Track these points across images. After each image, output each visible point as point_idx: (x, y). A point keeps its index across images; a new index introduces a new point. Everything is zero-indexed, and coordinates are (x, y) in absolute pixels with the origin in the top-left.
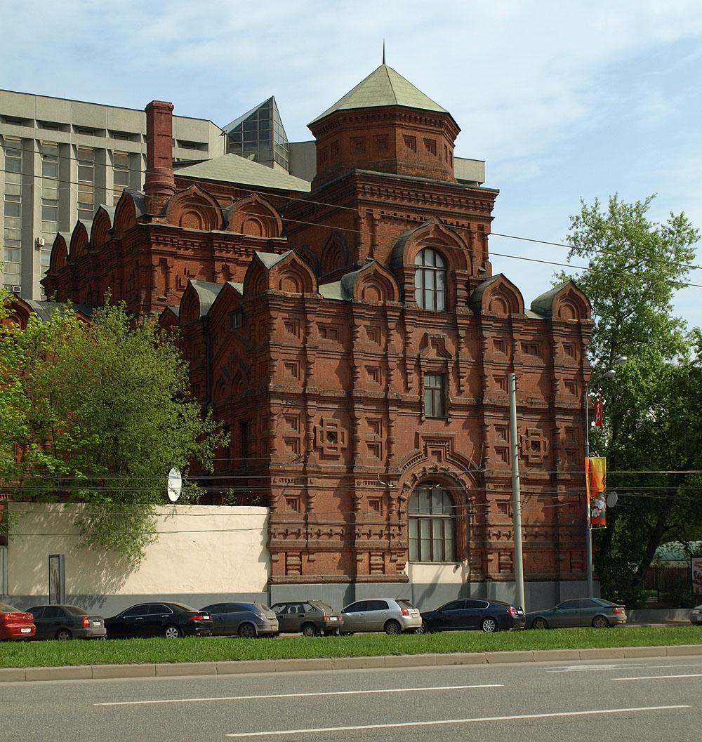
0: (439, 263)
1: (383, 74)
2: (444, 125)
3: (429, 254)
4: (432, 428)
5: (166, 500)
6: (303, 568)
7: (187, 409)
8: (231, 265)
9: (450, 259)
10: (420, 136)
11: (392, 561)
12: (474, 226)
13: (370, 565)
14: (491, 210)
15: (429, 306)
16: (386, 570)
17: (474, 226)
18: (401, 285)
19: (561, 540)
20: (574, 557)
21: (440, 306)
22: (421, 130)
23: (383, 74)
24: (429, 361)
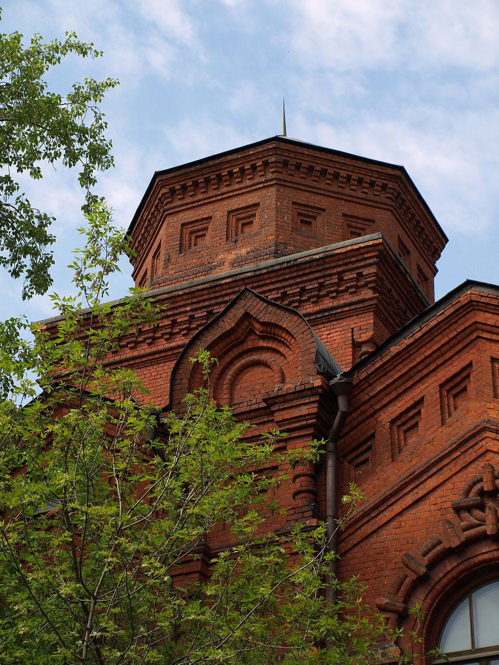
22: (339, 197)
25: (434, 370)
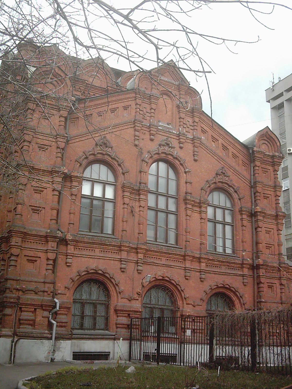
25: (128, 98)
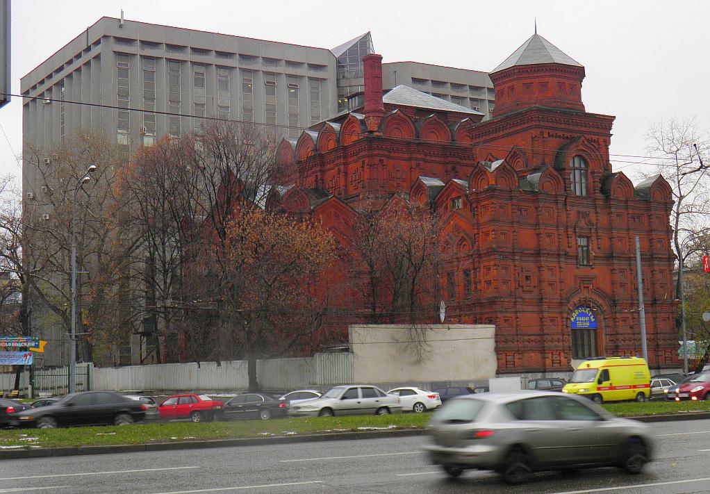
0: (583, 166)
1: (536, 42)
2: (578, 73)
3: (577, 160)
4: (582, 271)
5: (437, 321)
6: (516, 363)
7: (80, 432)
8: (458, 167)
9: (589, 160)
10: (568, 82)
11: (565, 358)
12: (601, 139)
13: (552, 361)
14: (610, 129)
15: (578, 193)
16: (562, 363)
17: (601, 139)
18: (131, 414)
19: (660, 343)
20: (554, 356)
21: (584, 193)
23: (536, 42)
24: (581, 228)
